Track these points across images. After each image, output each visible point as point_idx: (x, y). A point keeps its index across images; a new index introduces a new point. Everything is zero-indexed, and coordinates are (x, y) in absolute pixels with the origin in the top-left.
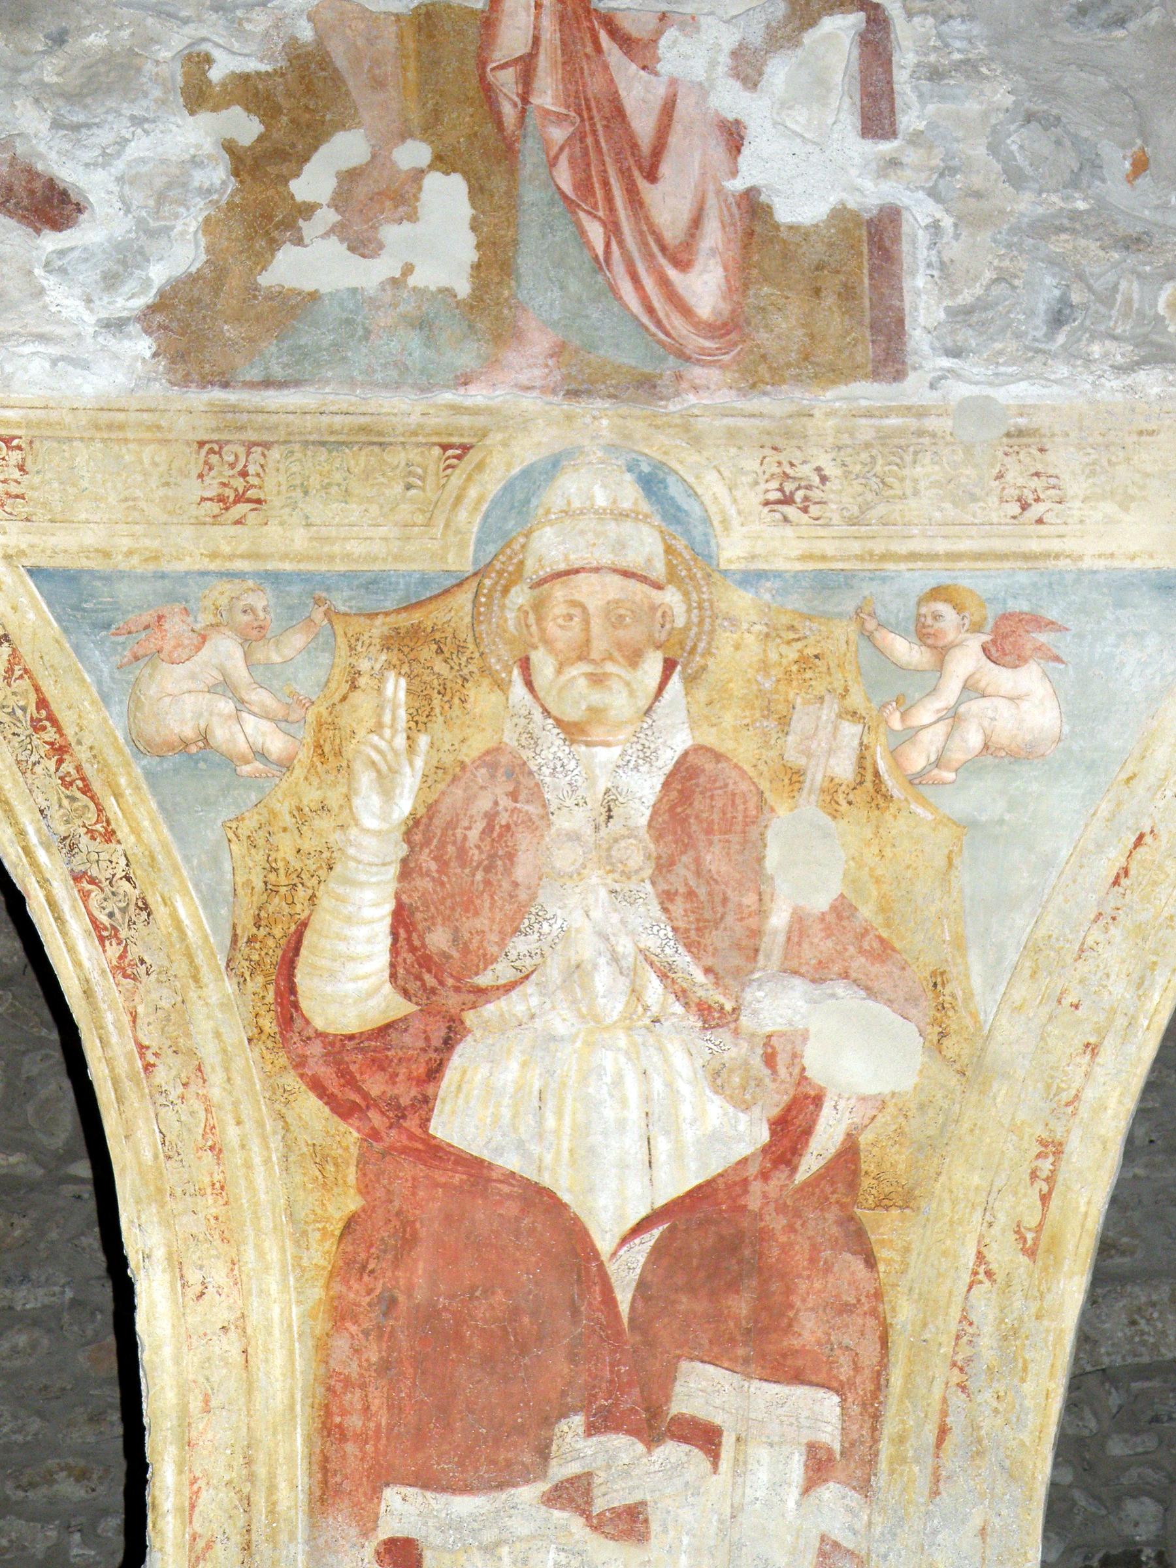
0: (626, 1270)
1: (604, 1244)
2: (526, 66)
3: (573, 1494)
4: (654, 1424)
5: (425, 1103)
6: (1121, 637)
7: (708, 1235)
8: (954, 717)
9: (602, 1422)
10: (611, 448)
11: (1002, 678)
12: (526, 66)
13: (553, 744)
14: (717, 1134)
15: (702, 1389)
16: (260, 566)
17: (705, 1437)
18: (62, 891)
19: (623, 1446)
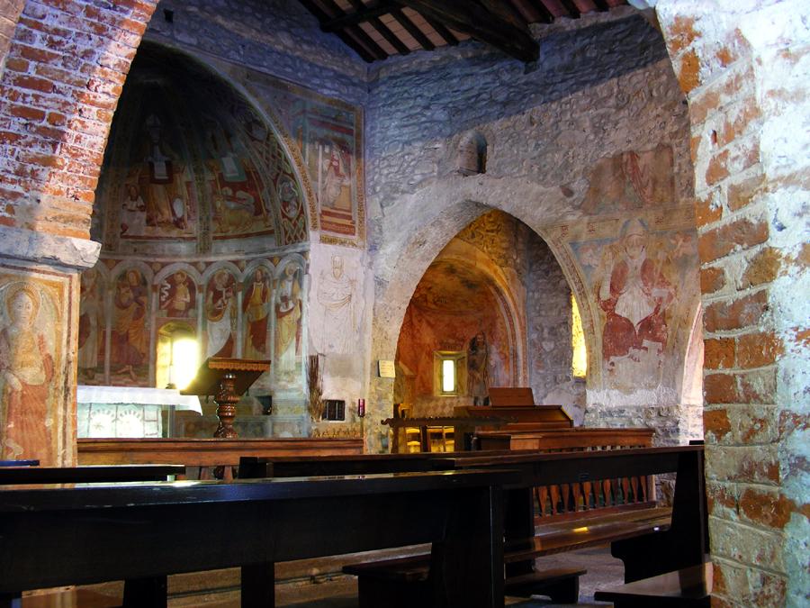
0: (637, 329)
1: (635, 325)
2: (626, 163)
3: (631, 357)
4: (640, 348)
5: (614, 309)
6: (501, 352)
7: (647, 324)
8: (679, 250)
9: (635, 348)
10: (609, 116)
11: (686, 244)
12: (626, 163)
13: (630, 260)
14: (648, 311)
15: (646, 343)
16: (337, 123)
17: (646, 349)
18: (574, 285)
19: (637, 350)
